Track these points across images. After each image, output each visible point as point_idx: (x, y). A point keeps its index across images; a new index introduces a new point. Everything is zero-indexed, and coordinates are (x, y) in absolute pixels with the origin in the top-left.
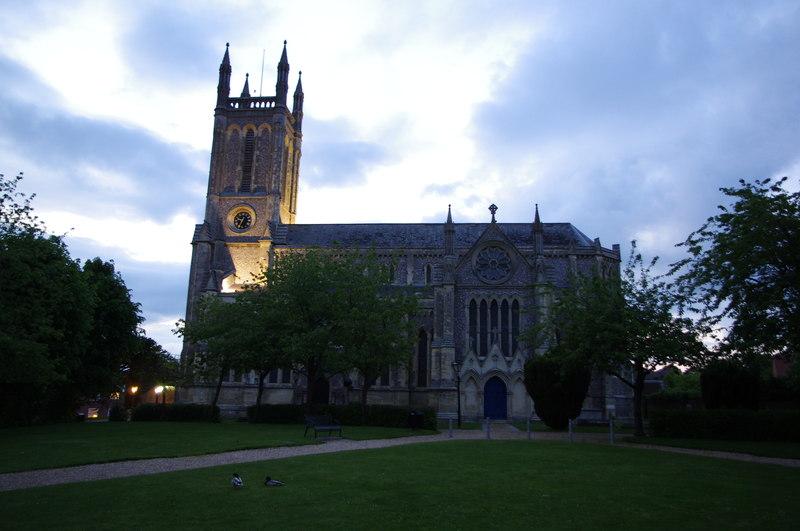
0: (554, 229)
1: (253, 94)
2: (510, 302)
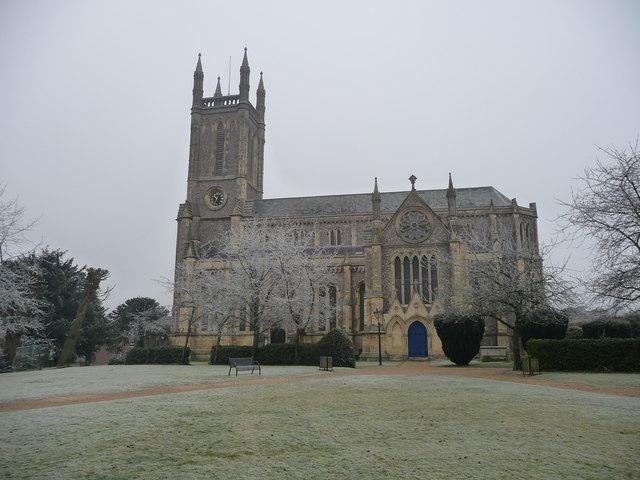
1: (224, 93)
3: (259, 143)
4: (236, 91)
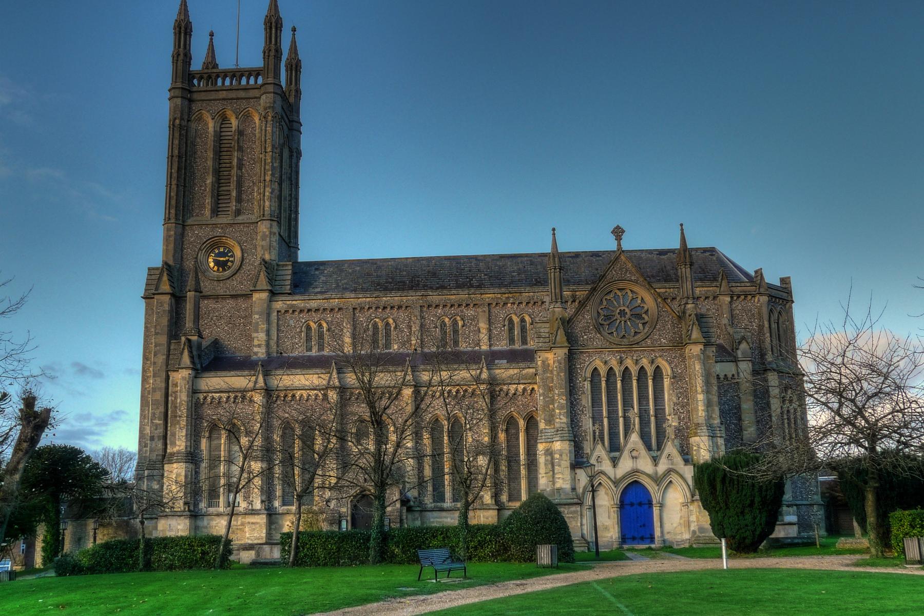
3: (291, 156)
4: (257, 61)
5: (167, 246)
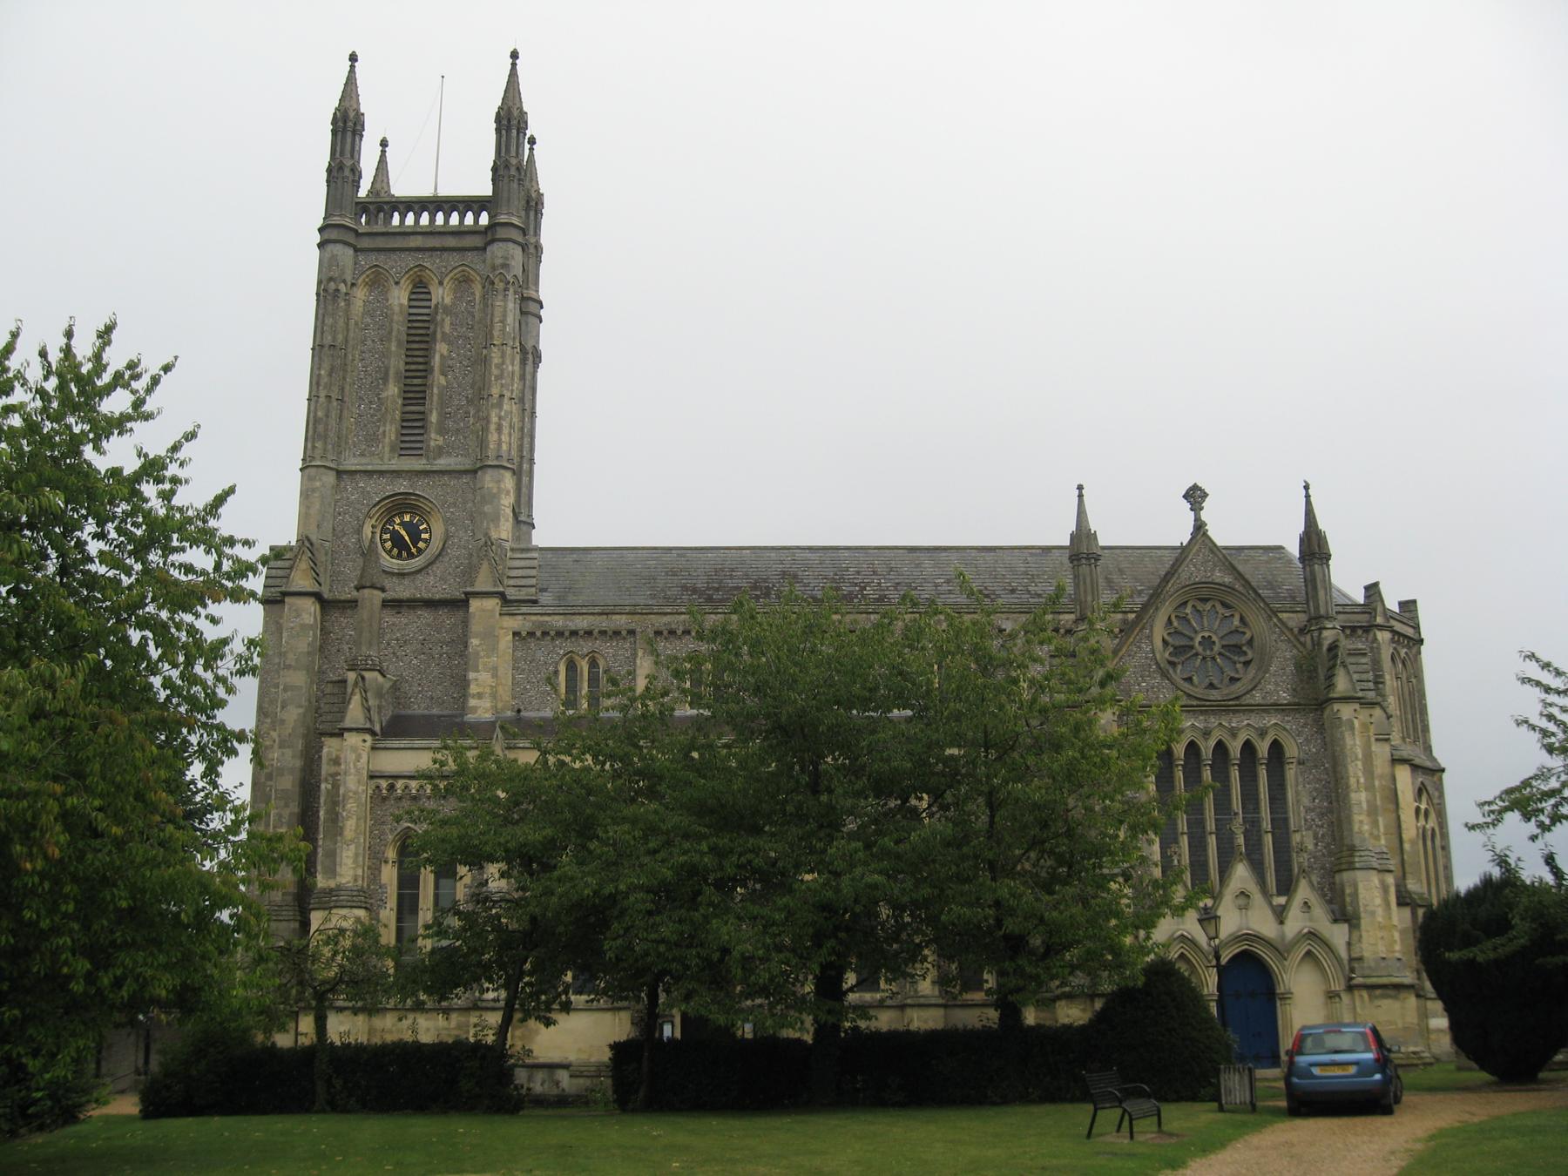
0: (631, 556)
1: (401, 187)
2: (1263, 748)
5: (308, 508)
